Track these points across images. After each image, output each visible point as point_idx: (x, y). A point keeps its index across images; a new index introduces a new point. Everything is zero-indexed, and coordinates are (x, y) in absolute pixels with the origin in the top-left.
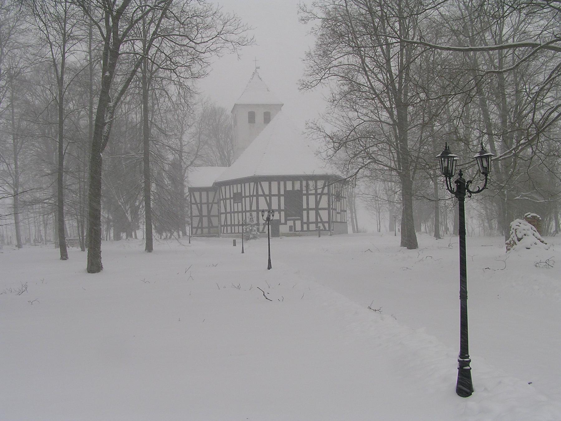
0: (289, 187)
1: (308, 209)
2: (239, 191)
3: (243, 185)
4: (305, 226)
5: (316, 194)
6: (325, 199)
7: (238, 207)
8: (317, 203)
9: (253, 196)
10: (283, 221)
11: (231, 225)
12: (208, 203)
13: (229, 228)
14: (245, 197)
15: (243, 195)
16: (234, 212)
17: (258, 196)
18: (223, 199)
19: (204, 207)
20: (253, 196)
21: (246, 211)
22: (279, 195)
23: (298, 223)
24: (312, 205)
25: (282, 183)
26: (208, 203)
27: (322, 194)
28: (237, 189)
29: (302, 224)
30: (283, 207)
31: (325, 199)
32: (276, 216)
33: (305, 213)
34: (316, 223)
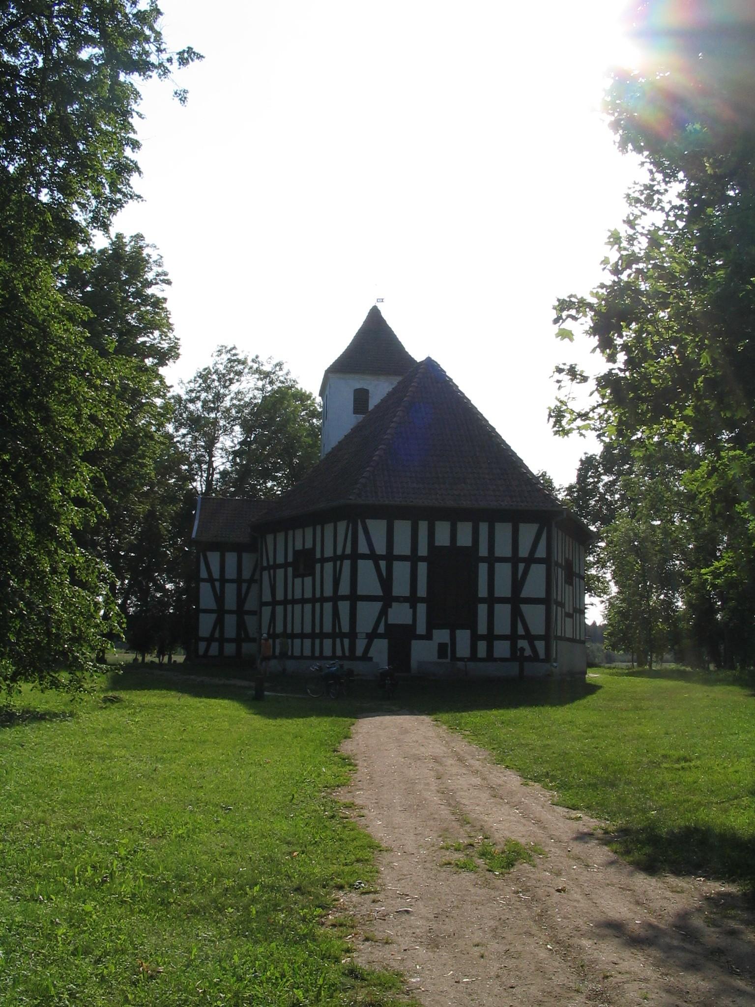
0: (443, 537)
1: (492, 600)
2: (309, 545)
3: (319, 528)
4: (482, 646)
5: (514, 560)
6: (538, 573)
7: (303, 587)
8: (517, 584)
9: (343, 557)
10: (421, 629)
11: (285, 635)
12: (239, 581)
13: (328, 643)
14: (323, 560)
15: (318, 556)
16: (294, 602)
17: (355, 557)
18: (269, 568)
19: (231, 591)
20: (343, 557)
21: (323, 600)
22: (413, 558)
23: (463, 637)
24: (503, 588)
25: (423, 526)
26: (514, 560)
27: (531, 560)
28: (303, 539)
29: (475, 638)
30: (422, 592)
31: (538, 573)
32: (400, 614)
33: (482, 609)
34: (513, 638)
